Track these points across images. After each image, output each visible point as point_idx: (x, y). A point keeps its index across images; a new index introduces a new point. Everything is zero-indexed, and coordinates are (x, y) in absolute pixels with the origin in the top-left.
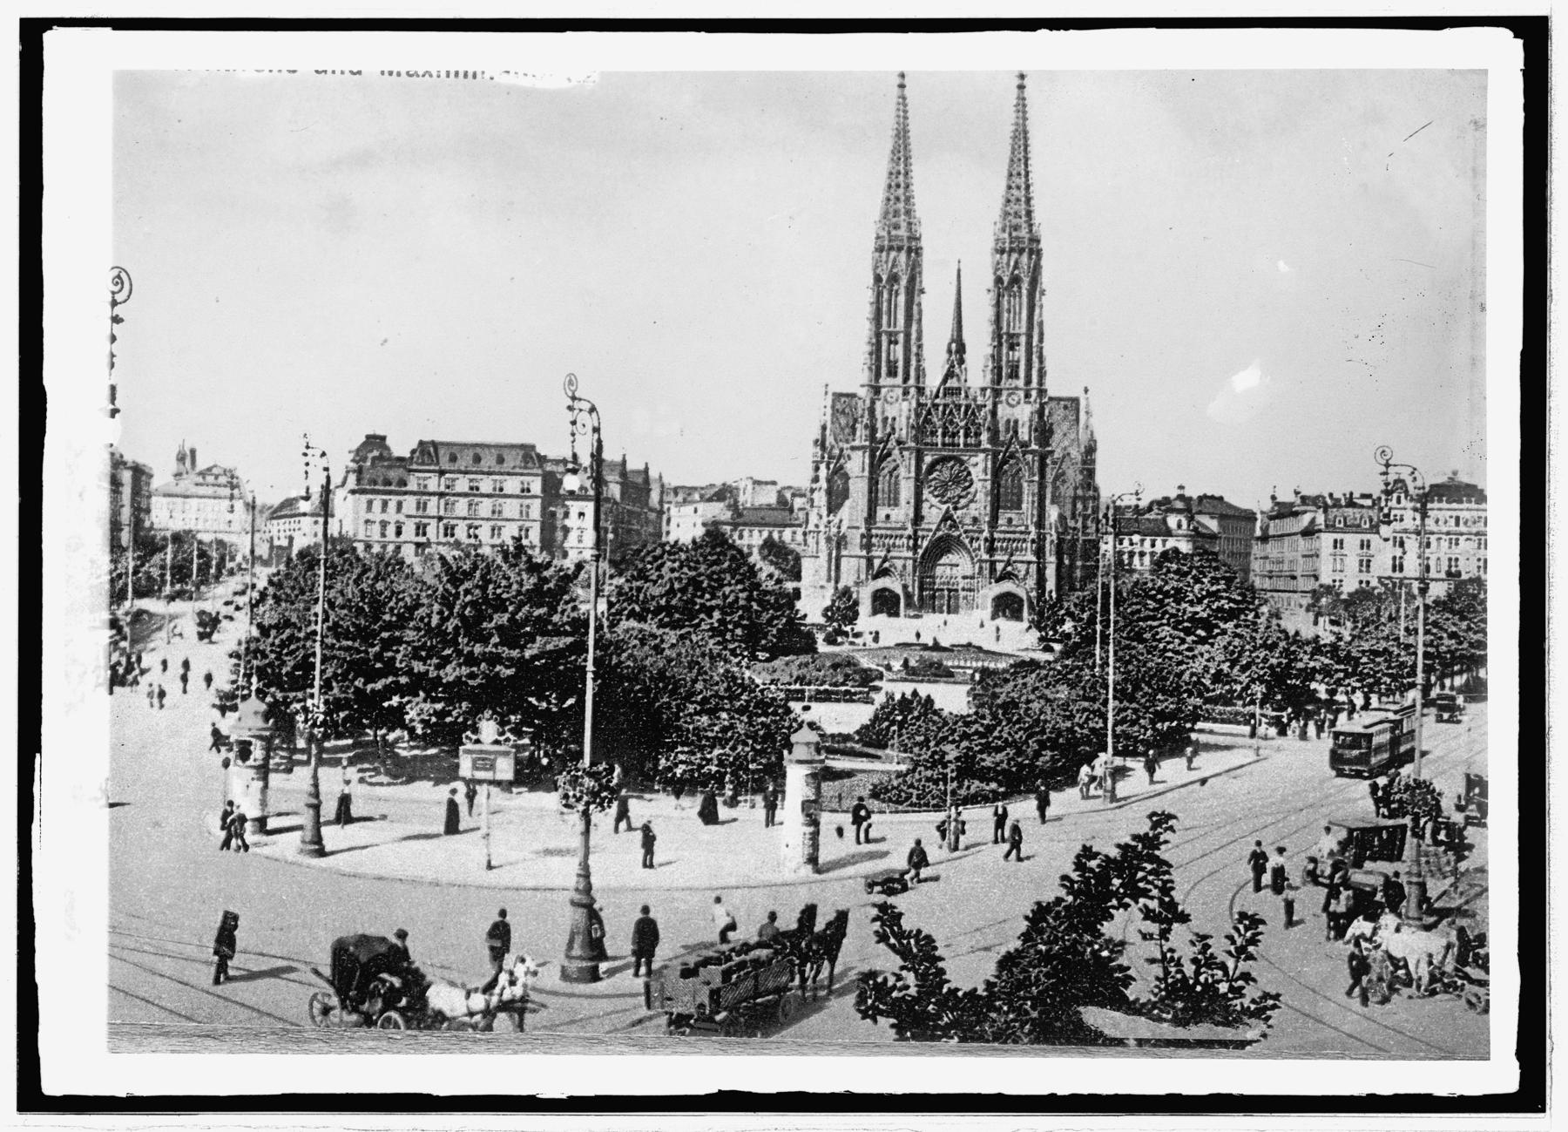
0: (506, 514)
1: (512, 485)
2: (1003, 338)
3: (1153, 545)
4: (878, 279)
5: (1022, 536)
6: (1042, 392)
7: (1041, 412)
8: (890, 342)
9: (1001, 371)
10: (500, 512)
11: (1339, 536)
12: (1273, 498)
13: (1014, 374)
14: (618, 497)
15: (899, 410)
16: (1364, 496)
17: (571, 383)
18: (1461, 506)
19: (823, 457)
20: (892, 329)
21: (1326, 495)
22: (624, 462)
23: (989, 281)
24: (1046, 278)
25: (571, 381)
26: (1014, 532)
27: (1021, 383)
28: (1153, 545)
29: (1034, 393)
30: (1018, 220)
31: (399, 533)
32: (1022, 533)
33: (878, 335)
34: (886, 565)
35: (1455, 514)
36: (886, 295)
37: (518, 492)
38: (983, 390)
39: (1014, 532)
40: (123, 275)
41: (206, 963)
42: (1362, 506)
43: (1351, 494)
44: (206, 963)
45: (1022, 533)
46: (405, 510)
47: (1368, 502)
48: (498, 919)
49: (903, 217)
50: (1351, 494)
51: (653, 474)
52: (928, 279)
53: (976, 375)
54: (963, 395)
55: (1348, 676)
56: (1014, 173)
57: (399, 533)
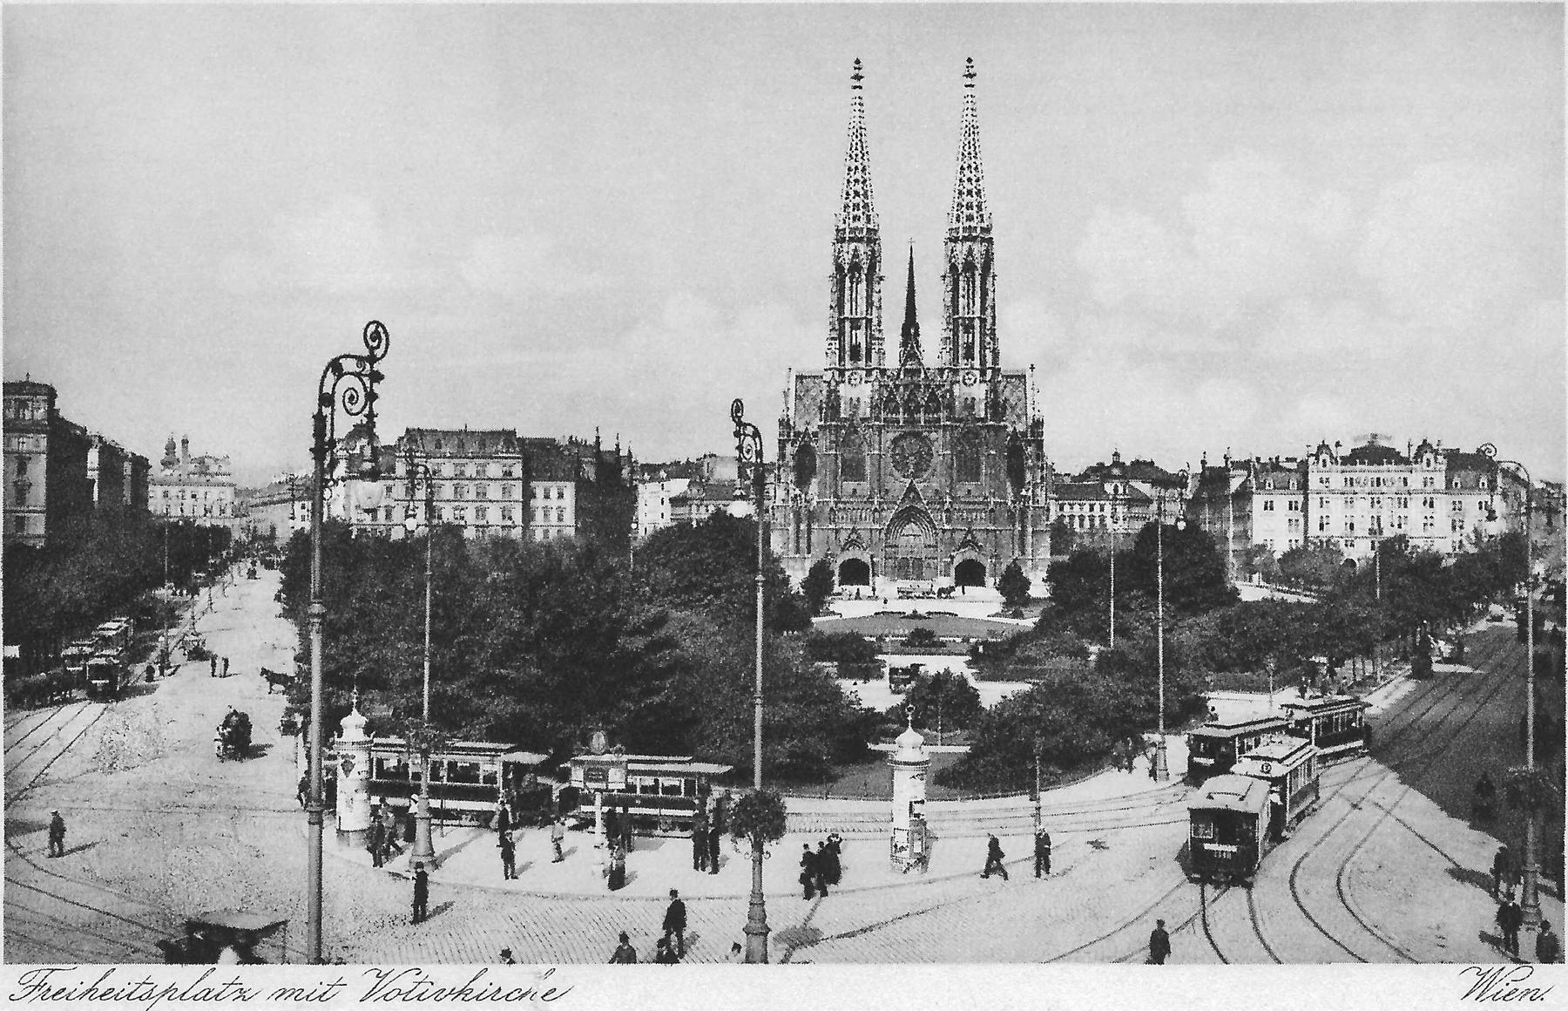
0: (489, 496)
1: (494, 469)
2: (957, 324)
3: (1092, 509)
4: (839, 268)
5: (982, 507)
6: (996, 371)
7: (994, 390)
8: (852, 328)
9: (959, 349)
10: (485, 494)
11: (1269, 498)
12: (1203, 462)
13: (969, 355)
14: (592, 477)
15: (859, 392)
16: (1288, 460)
17: (738, 411)
18: (1381, 467)
19: (789, 436)
20: (854, 316)
21: (1254, 460)
22: (598, 443)
23: (944, 267)
24: (996, 267)
25: (738, 407)
26: (974, 503)
27: (977, 363)
28: (1092, 509)
29: (989, 372)
30: (970, 211)
31: (388, 516)
32: (980, 503)
33: (841, 322)
34: (854, 536)
35: (1378, 475)
36: (848, 284)
37: (500, 475)
38: (941, 371)
39: (974, 503)
40: (380, 329)
41: (1406, 791)
42: (1290, 470)
43: (1277, 458)
44: (1406, 791)
45: (980, 503)
46: (394, 494)
47: (1293, 466)
48: (804, 851)
49: (862, 210)
50: (1277, 458)
51: (624, 453)
52: (884, 269)
53: (933, 351)
54: (923, 376)
55: (394, 560)
56: (965, 166)
57: (388, 516)
